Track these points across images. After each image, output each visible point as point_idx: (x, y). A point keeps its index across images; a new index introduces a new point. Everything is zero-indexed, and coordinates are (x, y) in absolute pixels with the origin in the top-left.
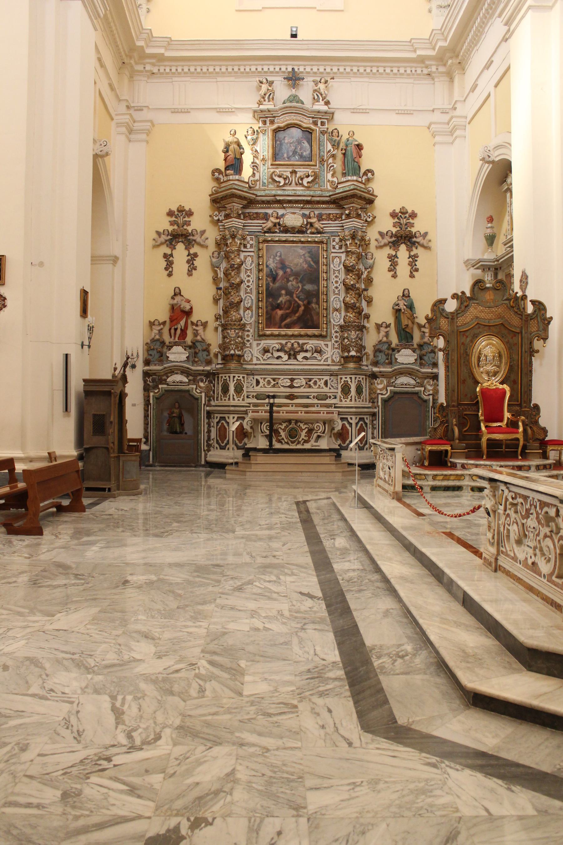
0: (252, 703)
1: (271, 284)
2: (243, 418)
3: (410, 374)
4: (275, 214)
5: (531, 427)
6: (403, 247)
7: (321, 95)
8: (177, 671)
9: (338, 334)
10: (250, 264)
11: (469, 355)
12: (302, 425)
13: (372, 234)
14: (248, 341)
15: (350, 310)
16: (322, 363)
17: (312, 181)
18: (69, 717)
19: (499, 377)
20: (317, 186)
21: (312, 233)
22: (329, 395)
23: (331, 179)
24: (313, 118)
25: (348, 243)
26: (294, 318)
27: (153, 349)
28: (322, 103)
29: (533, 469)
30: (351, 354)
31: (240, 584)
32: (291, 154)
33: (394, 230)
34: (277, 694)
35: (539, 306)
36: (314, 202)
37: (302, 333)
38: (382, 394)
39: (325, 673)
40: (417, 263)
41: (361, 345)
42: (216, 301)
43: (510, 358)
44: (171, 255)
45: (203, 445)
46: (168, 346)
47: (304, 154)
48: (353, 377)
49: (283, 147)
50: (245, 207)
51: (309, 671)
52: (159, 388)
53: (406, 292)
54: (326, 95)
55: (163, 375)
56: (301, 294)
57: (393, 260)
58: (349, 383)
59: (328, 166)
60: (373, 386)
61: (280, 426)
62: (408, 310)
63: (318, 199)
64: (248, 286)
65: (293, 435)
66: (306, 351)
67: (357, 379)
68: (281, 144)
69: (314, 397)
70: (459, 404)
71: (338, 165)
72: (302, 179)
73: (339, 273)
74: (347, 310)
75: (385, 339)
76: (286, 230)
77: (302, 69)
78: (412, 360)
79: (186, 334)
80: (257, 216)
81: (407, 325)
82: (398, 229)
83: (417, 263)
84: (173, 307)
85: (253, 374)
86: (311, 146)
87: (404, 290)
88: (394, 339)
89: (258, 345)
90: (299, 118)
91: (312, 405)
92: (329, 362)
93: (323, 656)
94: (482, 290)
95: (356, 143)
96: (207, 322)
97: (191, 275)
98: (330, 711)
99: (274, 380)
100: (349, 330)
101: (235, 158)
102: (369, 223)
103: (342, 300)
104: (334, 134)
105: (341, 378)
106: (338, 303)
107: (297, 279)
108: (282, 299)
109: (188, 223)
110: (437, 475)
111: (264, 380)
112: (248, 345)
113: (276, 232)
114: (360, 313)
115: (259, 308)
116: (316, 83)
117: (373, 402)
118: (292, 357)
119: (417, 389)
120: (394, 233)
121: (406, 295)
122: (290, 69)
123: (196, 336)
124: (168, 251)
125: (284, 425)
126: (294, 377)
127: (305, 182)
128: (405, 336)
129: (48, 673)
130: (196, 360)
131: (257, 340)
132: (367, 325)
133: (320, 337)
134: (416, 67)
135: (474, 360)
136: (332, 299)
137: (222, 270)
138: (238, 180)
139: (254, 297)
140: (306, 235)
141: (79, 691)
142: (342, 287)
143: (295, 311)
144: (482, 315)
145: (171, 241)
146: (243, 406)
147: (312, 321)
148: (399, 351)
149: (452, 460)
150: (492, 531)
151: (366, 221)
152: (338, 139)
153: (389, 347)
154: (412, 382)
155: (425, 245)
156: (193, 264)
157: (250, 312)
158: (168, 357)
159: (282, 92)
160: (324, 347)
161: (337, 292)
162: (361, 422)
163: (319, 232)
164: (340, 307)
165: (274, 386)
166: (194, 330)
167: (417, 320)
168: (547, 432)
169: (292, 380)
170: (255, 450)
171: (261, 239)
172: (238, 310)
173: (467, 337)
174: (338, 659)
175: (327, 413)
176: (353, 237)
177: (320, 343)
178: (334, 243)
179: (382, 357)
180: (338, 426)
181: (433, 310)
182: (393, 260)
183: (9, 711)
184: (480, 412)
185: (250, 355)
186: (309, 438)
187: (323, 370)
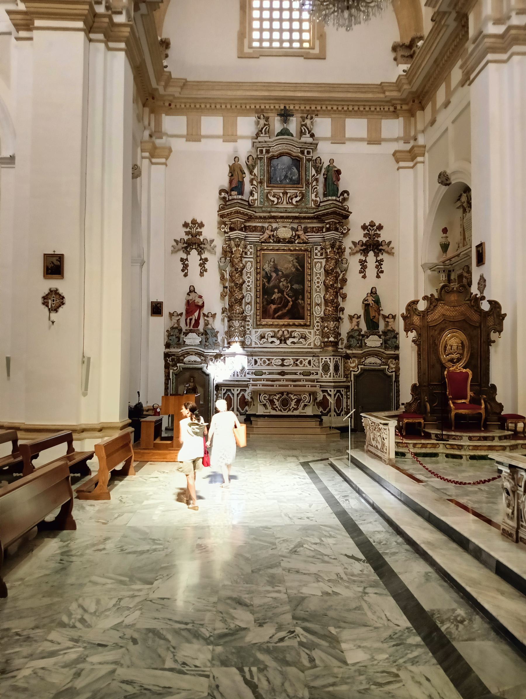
0: (360, 674)
1: (267, 284)
2: (245, 390)
3: (376, 355)
4: (270, 228)
5: (489, 403)
6: (371, 254)
7: (308, 129)
8: (282, 640)
9: (319, 324)
10: (250, 268)
11: (437, 345)
12: (292, 396)
13: (347, 243)
14: (248, 329)
15: (329, 304)
16: (306, 346)
17: (300, 200)
18: (213, 693)
19: (462, 363)
21: (298, 243)
22: (312, 372)
23: (314, 199)
24: (300, 148)
25: (328, 251)
26: (285, 311)
27: (173, 335)
28: (308, 135)
29: (497, 439)
30: (330, 340)
31: (293, 546)
32: (283, 178)
33: (365, 240)
34: (375, 662)
35: (495, 305)
36: (301, 217)
39: (406, 640)
41: (338, 333)
42: (223, 296)
43: (471, 347)
44: (187, 260)
46: (184, 333)
47: (294, 178)
48: (332, 358)
49: (277, 172)
50: (246, 221)
51: (391, 637)
52: (177, 367)
54: (312, 129)
55: (181, 356)
56: (290, 292)
57: (363, 265)
59: (312, 188)
61: (275, 397)
63: (304, 215)
64: (248, 286)
65: (285, 403)
66: (294, 337)
67: (335, 359)
68: (275, 170)
69: (300, 374)
70: (429, 385)
71: (320, 188)
72: (292, 199)
73: (320, 275)
74: (326, 305)
75: (356, 328)
76: (278, 241)
77: (292, 107)
78: (378, 344)
79: (199, 323)
80: (255, 229)
81: (375, 317)
82: (368, 239)
84: (188, 302)
86: (299, 171)
87: (372, 288)
88: (363, 327)
89: (256, 332)
90: (289, 148)
91: (299, 380)
92: (312, 346)
93: (397, 622)
94: (448, 292)
95: (336, 169)
96: (215, 314)
98: (428, 680)
99: (269, 360)
100: (329, 321)
101: (239, 181)
102: (345, 235)
103: (322, 296)
104: (317, 161)
107: (287, 280)
108: (275, 296)
109: (200, 234)
110: (416, 444)
111: (261, 360)
112: (248, 332)
113: (270, 242)
114: (337, 307)
115: (257, 303)
116: (303, 119)
117: (347, 378)
118: (283, 342)
119: (382, 367)
120: (364, 242)
121: (373, 292)
122: (282, 107)
123: (207, 325)
124: (184, 256)
125: (278, 396)
126: (284, 358)
128: (372, 325)
129: (174, 645)
132: (342, 316)
133: (305, 326)
134: (384, 106)
135: (441, 349)
136: (314, 296)
137: (228, 272)
138: (241, 199)
140: (294, 245)
141: (209, 664)
142: (322, 286)
144: (448, 313)
146: (245, 381)
148: (368, 337)
149: (427, 430)
150: (511, 507)
152: (321, 165)
153: (359, 335)
154: (379, 361)
155: (389, 251)
156: (204, 267)
159: (277, 125)
161: (318, 290)
163: (304, 243)
164: (321, 302)
165: (269, 365)
167: (382, 312)
168: (503, 407)
169: (283, 360)
170: (255, 415)
171: (259, 248)
172: (241, 305)
173: (435, 330)
174: (409, 625)
175: (311, 386)
176: (333, 246)
177: (305, 331)
178: (317, 251)
179: (353, 342)
180: (320, 397)
181: (407, 310)
182: (363, 265)
183: (157, 688)
184: (448, 390)
185: (250, 340)
186: (298, 407)
187: (307, 352)
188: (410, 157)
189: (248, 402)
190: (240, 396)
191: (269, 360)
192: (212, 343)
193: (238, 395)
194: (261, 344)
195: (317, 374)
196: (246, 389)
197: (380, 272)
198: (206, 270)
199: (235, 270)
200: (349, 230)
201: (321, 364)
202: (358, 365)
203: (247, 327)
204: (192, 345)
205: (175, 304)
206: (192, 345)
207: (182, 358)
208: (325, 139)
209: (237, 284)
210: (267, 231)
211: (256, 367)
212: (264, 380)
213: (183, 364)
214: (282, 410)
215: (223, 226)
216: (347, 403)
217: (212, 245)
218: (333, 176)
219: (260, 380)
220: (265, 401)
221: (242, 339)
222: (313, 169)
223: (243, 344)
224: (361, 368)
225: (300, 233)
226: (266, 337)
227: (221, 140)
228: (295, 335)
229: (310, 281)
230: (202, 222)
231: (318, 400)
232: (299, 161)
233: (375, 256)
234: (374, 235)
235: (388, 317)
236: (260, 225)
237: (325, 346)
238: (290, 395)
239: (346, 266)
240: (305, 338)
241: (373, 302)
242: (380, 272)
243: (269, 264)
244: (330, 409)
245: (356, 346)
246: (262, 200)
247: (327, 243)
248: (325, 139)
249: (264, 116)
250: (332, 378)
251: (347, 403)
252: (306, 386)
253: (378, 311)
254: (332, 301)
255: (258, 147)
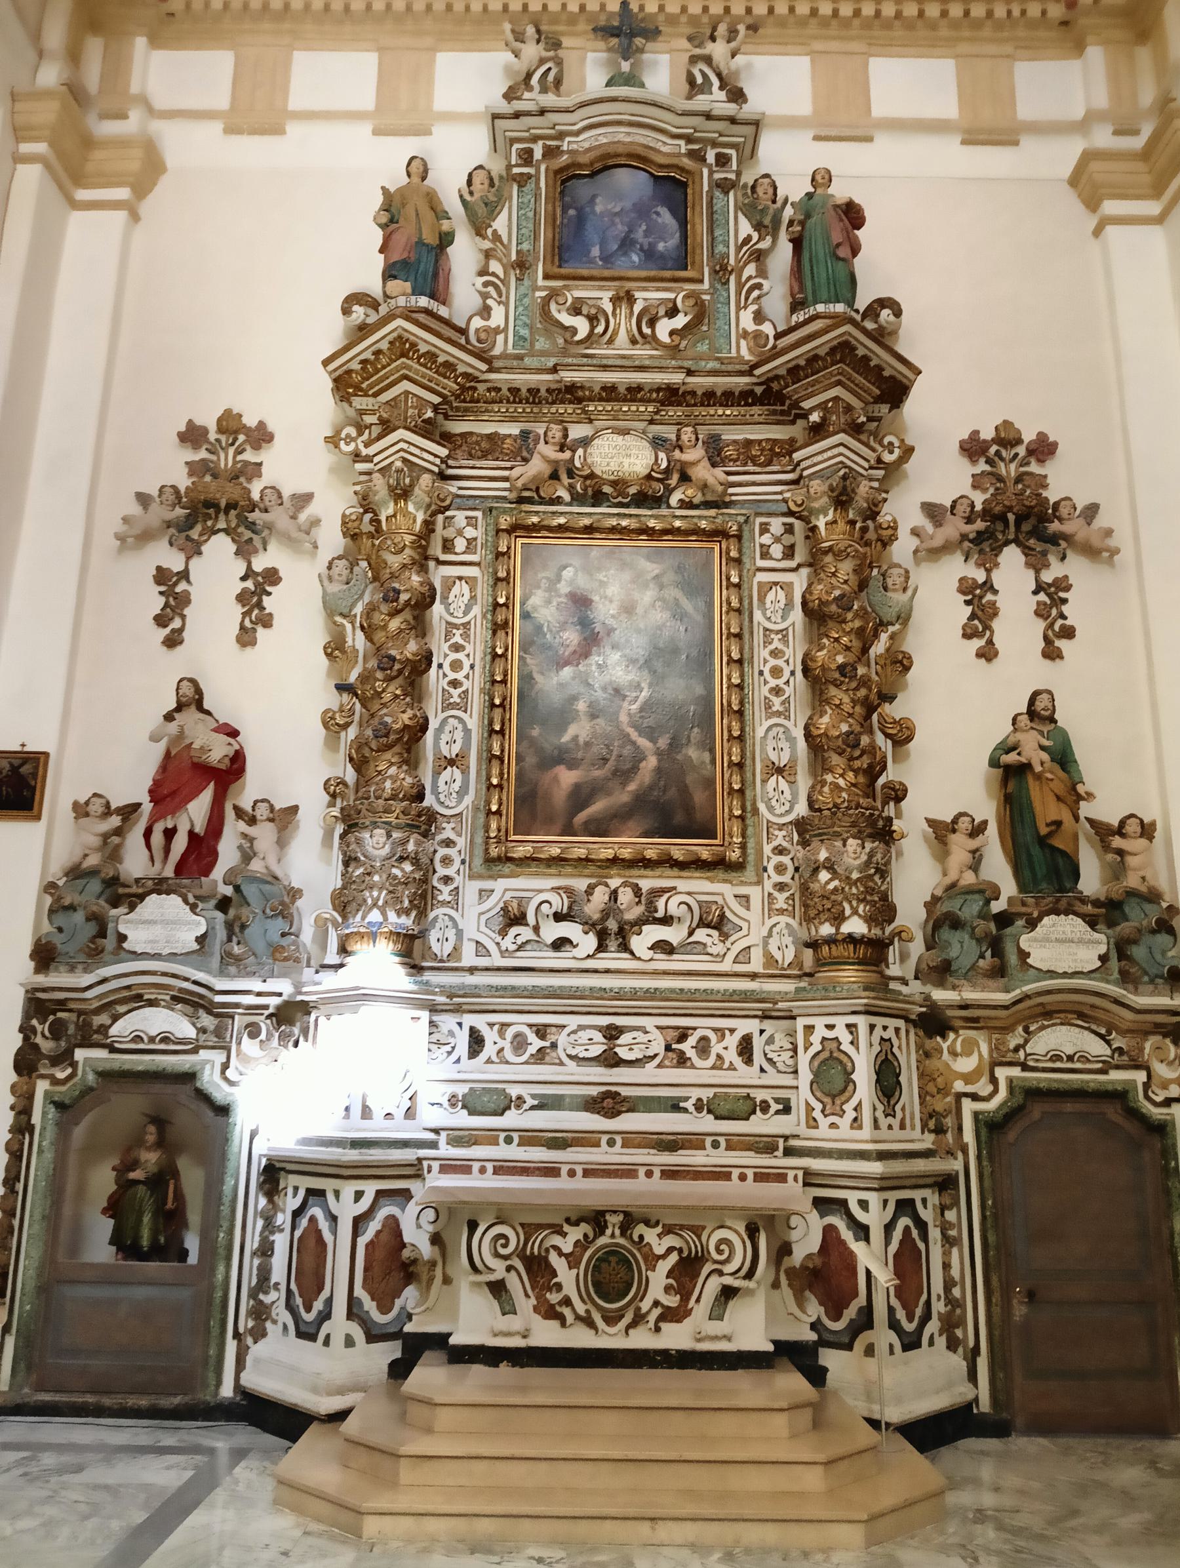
3: (1081, 1016)
6: (1011, 557)
9: (786, 860)
12: (651, 1236)
13: (904, 509)
14: (447, 880)
15: (835, 760)
16: (727, 966)
17: (686, 327)
20: (703, 348)
21: (686, 504)
22: (759, 1095)
30: (846, 928)
37: (651, 854)
38: (975, 1097)
40: (1065, 609)
44: (185, 575)
45: (238, 1315)
47: (661, 246)
48: (862, 1021)
52: (74, 1065)
53: (1040, 705)
58: (846, 1047)
59: (740, 286)
60: (933, 1064)
61: (557, 1240)
62: (1057, 768)
65: (613, 1279)
66: (667, 920)
67: (878, 1031)
72: (652, 323)
73: (785, 640)
75: (969, 878)
80: (491, 447)
81: (1058, 824)
83: (1065, 609)
85: (458, 1010)
86: (683, 223)
89: (484, 894)
91: (693, 1141)
96: (294, 809)
97: (253, 643)
99: (541, 1031)
100: (837, 835)
103: (799, 733)
105: (809, 1029)
106: (785, 745)
111: (501, 1034)
112: (445, 894)
113: (558, 501)
117: (939, 1131)
118: (613, 944)
119: (1115, 1075)
120: (979, 507)
121: (1039, 712)
124: (174, 561)
125: (575, 1234)
127: (663, 329)
128: (1046, 869)
130: (237, 950)
131: (480, 877)
133: (719, 865)
136: (760, 732)
139: (473, 722)
140: (664, 511)
143: (624, 774)
145: (185, 525)
146: (405, 1144)
147: (689, 808)
148: (1032, 924)
151: (879, 460)
154: (1097, 1048)
155: (1096, 542)
156: (259, 605)
157: (457, 774)
158: (122, 938)
159: (591, 70)
160: (734, 904)
162: (904, 1221)
163: (707, 505)
165: (540, 1057)
166: (245, 836)
169: (612, 1033)
171: (505, 522)
175: (760, 1177)
176: (842, 499)
178: (766, 539)
180: (806, 1241)
185: (451, 934)
186: (685, 1298)
187: (732, 996)
188: (1146, 179)
189: (414, 1261)
190: (374, 1227)
191: (541, 1031)
192: (260, 946)
193: (359, 1223)
194: (504, 953)
195: (787, 1110)
196: (413, 1186)
197: (1056, 638)
198: (267, 621)
199: (386, 599)
200: (908, 451)
201: (804, 1059)
202: (994, 1064)
203: (441, 871)
204: (156, 956)
205: (106, 759)
206: (156, 956)
207: (98, 1020)
208: (791, 123)
209: (393, 659)
210: (541, 446)
211: (479, 1071)
212: (508, 1141)
213: (102, 1054)
214: (597, 1317)
215: (353, 431)
216: (946, 1266)
217: (303, 517)
218: (827, 234)
219: (490, 1137)
220: (499, 1266)
221: (407, 921)
222: (743, 221)
223: (411, 950)
224: (1010, 1081)
225: (694, 454)
226: (531, 919)
227: (366, 128)
228: (673, 909)
229: (740, 662)
230: (262, 425)
231: (798, 1256)
232: (684, 185)
233: (1028, 565)
234: (1019, 479)
235: (1120, 831)
236: (514, 429)
237: (820, 963)
238: (641, 1229)
239: (904, 598)
240: (719, 923)
241: (1045, 756)
242: (1056, 638)
243: (549, 590)
244: (867, 1312)
245: (973, 967)
246: (525, 332)
247: (817, 486)
248: (791, 123)
249: (538, 31)
250: (867, 1132)
251: (946, 1266)
252: (727, 1176)
253: (1073, 796)
254: (851, 741)
255: (513, 141)
